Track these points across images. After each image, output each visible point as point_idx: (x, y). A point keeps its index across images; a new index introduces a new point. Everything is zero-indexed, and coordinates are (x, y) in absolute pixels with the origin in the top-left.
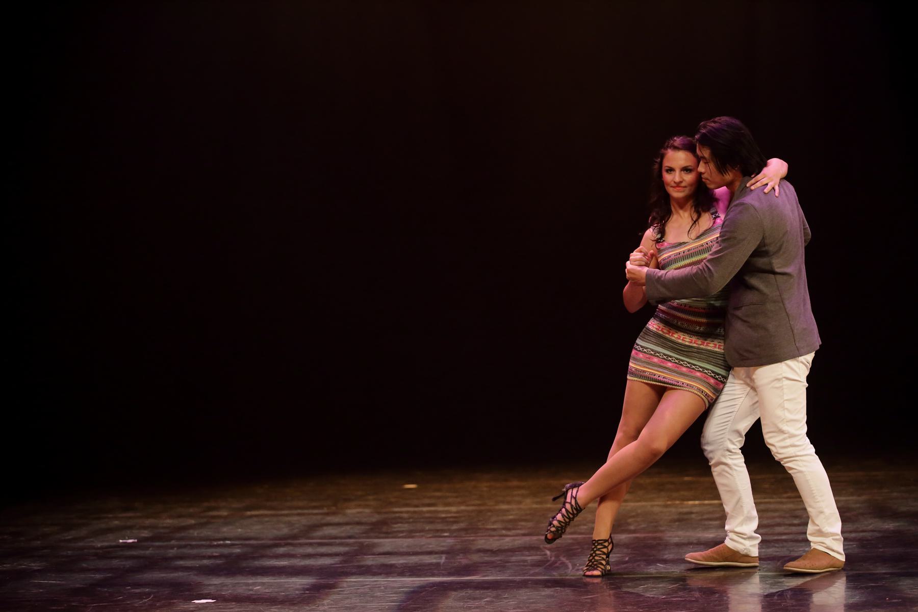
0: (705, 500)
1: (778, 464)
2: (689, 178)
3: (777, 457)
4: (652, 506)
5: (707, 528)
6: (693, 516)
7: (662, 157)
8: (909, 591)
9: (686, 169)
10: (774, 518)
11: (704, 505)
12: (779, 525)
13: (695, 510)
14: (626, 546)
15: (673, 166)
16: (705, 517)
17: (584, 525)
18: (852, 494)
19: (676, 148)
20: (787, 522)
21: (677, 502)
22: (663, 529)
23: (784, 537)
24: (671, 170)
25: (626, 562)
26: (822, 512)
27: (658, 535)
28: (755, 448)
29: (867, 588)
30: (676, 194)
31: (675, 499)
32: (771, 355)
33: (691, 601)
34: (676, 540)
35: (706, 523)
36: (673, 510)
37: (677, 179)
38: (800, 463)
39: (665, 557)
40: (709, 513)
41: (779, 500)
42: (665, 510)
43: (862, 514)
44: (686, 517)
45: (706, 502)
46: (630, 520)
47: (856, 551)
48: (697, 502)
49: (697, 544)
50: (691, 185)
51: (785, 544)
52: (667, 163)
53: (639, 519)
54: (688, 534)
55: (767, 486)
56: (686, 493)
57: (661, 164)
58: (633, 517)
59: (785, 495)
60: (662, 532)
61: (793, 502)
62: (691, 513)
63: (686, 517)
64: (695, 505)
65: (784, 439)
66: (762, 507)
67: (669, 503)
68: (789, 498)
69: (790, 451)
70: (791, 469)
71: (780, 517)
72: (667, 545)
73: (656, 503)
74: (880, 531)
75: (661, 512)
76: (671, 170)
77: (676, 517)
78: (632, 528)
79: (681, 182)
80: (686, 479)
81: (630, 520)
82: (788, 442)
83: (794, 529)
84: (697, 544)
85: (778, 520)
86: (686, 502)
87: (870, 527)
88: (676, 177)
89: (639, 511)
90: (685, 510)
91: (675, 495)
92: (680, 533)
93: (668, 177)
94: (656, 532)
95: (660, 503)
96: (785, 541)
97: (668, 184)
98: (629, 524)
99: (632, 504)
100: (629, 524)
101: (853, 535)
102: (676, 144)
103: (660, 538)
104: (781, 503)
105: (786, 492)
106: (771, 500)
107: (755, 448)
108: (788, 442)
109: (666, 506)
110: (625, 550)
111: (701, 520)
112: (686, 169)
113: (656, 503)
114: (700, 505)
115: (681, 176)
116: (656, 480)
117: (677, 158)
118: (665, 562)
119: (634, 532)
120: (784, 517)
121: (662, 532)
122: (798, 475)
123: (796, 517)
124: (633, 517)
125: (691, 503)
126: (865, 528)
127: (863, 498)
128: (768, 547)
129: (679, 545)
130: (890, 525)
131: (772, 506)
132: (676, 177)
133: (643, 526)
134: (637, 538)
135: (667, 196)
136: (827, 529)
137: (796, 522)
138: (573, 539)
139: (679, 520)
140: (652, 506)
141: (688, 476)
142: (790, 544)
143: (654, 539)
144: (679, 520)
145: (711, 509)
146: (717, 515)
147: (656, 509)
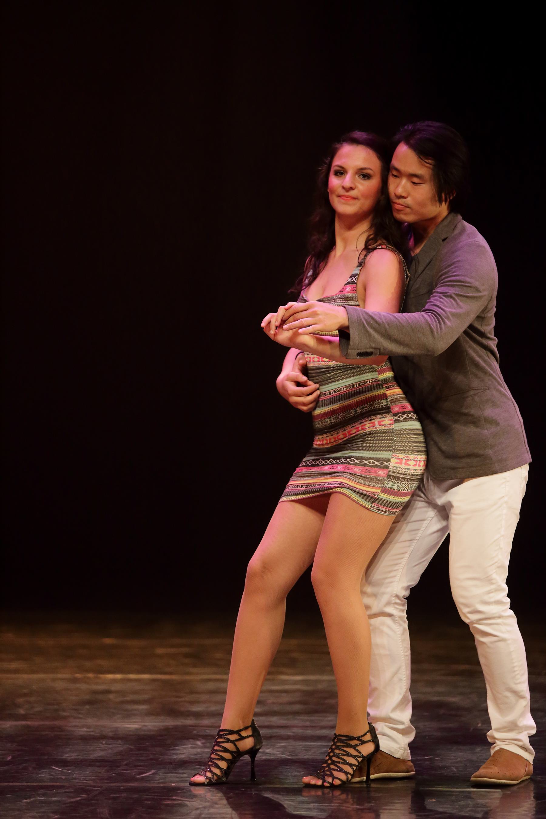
1: (466, 626)
3: (467, 615)
4: (54, 680)
5: (128, 715)
6: (111, 696)
7: (332, 154)
9: (365, 175)
11: (130, 680)
16: (129, 698)
19: (355, 141)
21: (91, 675)
22: (64, 714)
25: (8, 763)
27: (57, 723)
28: (432, 602)
30: (344, 207)
31: (87, 671)
32: (483, 465)
34: (83, 731)
35: (129, 707)
36: (83, 686)
38: (503, 628)
39: (65, 756)
40: (135, 692)
42: (72, 686)
44: (100, 697)
45: (132, 676)
46: (20, 700)
48: (118, 676)
49: (112, 738)
50: (365, 196)
52: (337, 162)
53: (32, 699)
58: (25, 695)
60: (65, 718)
62: (109, 692)
64: (115, 681)
65: (489, 592)
66: (434, 694)
67: (78, 676)
70: (485, 634)
73: (60, 676)
75: (66, 690)
76: (341, 172)
77: (87, 697)
78: (22, 711)
79: (352, 189)
80: (108, 641)
81: (20, 700)
84: (112, 738)
86: (102, 676)
89: (34, 687)
91: (88, 664)
92: (90, 721)
93: (334, 181)
94: (54, 719)
97: (333, 192)
99: (25, 676)
107: (432, 602)
109: (75, 681)
111: (122, 702)
112: (365, 175)
113: (60, 676)
114: (122, 680)
118: (64, 763)
119: (24, 717)
121: (65, 718)
122: (501, 644)
124: (25, 695)
125: (110, 676)
129: (86, 739)
133: (38, 709)
134: (28, 727)
135: (333, 212)
140: (54, 680)
141: (109, 636)
143: (52, 728)
144: (90, 702)
145: (137, 687)
146: (146, 697)
147: (59, 685)
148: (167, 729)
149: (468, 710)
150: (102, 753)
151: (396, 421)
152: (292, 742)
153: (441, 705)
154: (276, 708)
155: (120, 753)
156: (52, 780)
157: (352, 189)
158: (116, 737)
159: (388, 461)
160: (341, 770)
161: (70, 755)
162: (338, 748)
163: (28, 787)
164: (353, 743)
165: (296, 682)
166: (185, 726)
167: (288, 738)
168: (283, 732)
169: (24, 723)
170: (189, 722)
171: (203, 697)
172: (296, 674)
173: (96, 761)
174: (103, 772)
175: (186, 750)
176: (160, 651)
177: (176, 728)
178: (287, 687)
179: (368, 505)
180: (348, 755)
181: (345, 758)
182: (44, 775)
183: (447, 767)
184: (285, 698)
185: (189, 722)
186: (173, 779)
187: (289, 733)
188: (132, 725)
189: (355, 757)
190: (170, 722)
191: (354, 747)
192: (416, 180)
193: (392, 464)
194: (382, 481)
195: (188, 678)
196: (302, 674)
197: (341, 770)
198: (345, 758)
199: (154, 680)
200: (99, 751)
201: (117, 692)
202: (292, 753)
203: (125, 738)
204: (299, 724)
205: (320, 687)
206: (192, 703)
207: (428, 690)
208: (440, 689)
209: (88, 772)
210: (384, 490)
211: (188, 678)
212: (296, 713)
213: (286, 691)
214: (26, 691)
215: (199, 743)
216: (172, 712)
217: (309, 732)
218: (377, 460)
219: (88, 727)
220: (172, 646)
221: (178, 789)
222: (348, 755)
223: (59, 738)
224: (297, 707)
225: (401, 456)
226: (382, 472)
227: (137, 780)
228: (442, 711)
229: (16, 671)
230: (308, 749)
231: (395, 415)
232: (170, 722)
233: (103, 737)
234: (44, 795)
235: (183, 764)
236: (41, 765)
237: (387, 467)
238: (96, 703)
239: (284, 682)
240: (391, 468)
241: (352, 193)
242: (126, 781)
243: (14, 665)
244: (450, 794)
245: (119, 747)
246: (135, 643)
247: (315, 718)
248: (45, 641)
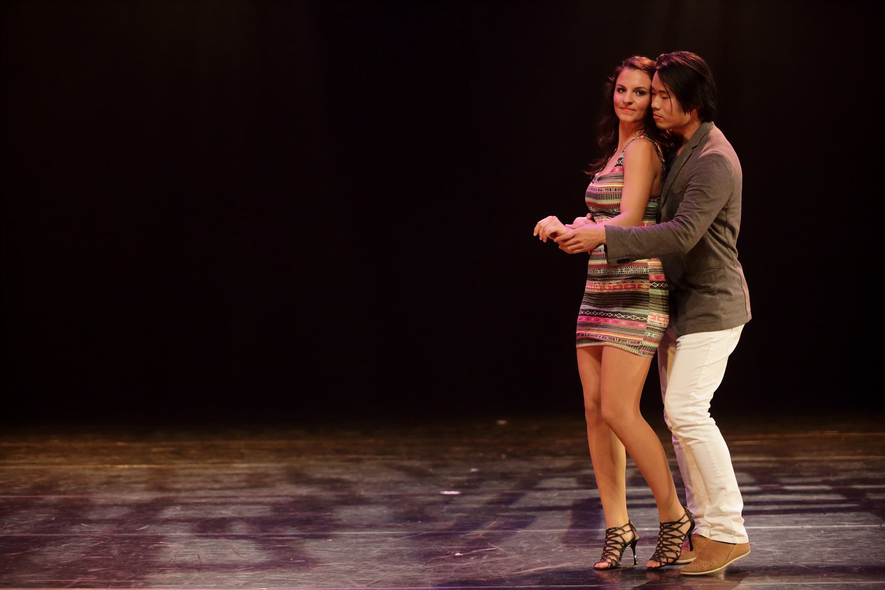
0: (134, 464)
2: (640, 101)
3: (669, 424)
4: (84, 469)
5: (132, 491)
6: (121, 479)
7: (617, 74)
8: (312, 552)
9: (639, 91)
10: (197, 482)
11: (134, 469)
12: (200, 489)
13: (123, 473)
14: (55, 506)
15: (625, 85)
16: (132, 480)
17: (17, 486)
18: (272, 461)
20: (209, 486)
21: (108, 466)
23: (204, 500)
24: (623, 89)
26: (723, 489)
27: (86, 496)
29: (274, 549)
30: (625, 117)
33: (109, 560)
35: (133, 486)
36: (103, 473)
37: (627, 100)
39: (90, 517)
40: (137, 476)
41: (203, 465)
43: (279, 480)
44: (114, 480)
45: (135, 466)
46: (61, 482)
47: (269, 514)
48: (126, 466)
50: (641, 109)
51: (204, 507)
52: (620, 82)
54: (115, 496)
55: (193, 452)
56: (117, 458)
57: (614, 83)
58: (65, 479)
59: (210, 461)
60: (90, 493)
61: (216, 468)
62: (119, 476)
63: (114, 480)
64: (124, 469)
67: (100, 466)
68: (214, 463)
69: (691, 419)
71: (202, 481)
72: (92, 507)
74: (293, 497)
76: (623, 89)
77: (105, 480)
78: (62, 489)
79: (630, 103)
80: (120, 444)
82: (690, 409)
83: (214, 493)
85: (200, 485)
87: (285, 493)
88: (626, 97)
89: (71, 474)
90: (114, 474)
91: (107, 459)
92: (107, 495)
93: (618, 97)
94: (83, 494)
95: (92, 466)
96: (205, 504)
97: (617, 105)
98: (59, 486)
100: (59, 486)
101: (269, 499)
102: (637, 63)
103: (87, 500)
104: (205, 468)
105: (210, 458)
106: (196, 466)
108: (690, 409)
109: (98, 469)
110: (53, 511)
111: (128, 483)
112: (639, 91)
114: (129, 469)
115: (631, 97)
116: (91, 444)
117: (632, 78)
118: (89, 522)
119: (64, 493)
120: (206, 482)
121: (90, 493)
123: (217, 482)
124: (65, 479)
125: (121, 466)
126: (280, 493)
127: (283, 465)
128: (188, 510)
129: (104, 506)
130: (304, 491)
131: (195, 472)
132: (626, 97)
133: (72, 488)
134: (66, 499)
135: (618, 120)
136: (725, 508)
137: (217, 486)
138: (4, 499)
139: (107, 483)
142: (208, 507)
143: (81, 500)
144: (107, 483)
146: (144, 479)
147: (88, 472)
148: (157, 500)
149: (356, 483)
150: (114, 515)
151: (652, 287)
152: (240, 507)
153: (337, 481)
154: (229, 485)
155: (126, 515)
156: (81, 532)
157: (630, 103)
158: (124, 505)
159: (646, 316)
160: (671, 551)
161: (93, 516)
162: (665, 533)
163: (50, 537)
164: (675, 526)
165: (244, 468)
166: (169, 498)
167: (237, 504)
168: (233, 500)
169: (63, 496)
170: (172, 494)
171: (182, 479)
172: (243, 463)
173: (109, 520)
174: (114, 527)
175: (169, 513)
176: (154, 450)
177: (163, 499)
178: (237, 472)
179: (636, 352)
180: (674, 537)
181: (673, 540)
182: (76, 529)
183: (340, 520)
184: (236, 479)
185: (172, 494)
186: (159, 530)
187: (238, 500)
188: (135, 497)
189: (679, 537)
190: (159, 495)
191: (677, 529)
192: (664, 96)
193: (649, 319)
194: (643, 332)
195: (171, 467)
196: (248, 462)
197: (671, 551)
198: (673, 540)
199: (150, 469)
200: (112, 514)
201: (125, 476)
202: (239, 513)
203: (129, 505)
204: (244, 495)
205: (259, 471)
206: (174, 482)
207: (331, 471)
208: (338, 470)
209: (105, 527)
210: (645, 339)
211: (171, 467)
212: (243, 488)
213: (237, 474)
214: (66, 476)
215: (178, 508)
216: (161, 489)
217: (251, 500)
218: (638, 315)
219: (106, 498)
220: (162, 447)
221: (163, 537)
222: (674, 537)
223: (90, 506)
224: (243, 484)
225: (655, 314)
226: (642, 325)
227: (136, 532)
228: (339, 485)
229: (60, 464)
230: (249, 510)
231: (651, 282)
232: (159, 495)
233: (116, 505)
234: (76, 541)
235: (167, 521)
236: (74, 523)
237: (646, 321)
238: (111, 483)
239: (236, 468)
240: (648, 322)
241: (631, 106)
242: (129, 532)
243: (58, 460)
244: (341, 536)
245: (126, 511)
246: (139, 445)
247: (255, 490)
248: (77, 445)
